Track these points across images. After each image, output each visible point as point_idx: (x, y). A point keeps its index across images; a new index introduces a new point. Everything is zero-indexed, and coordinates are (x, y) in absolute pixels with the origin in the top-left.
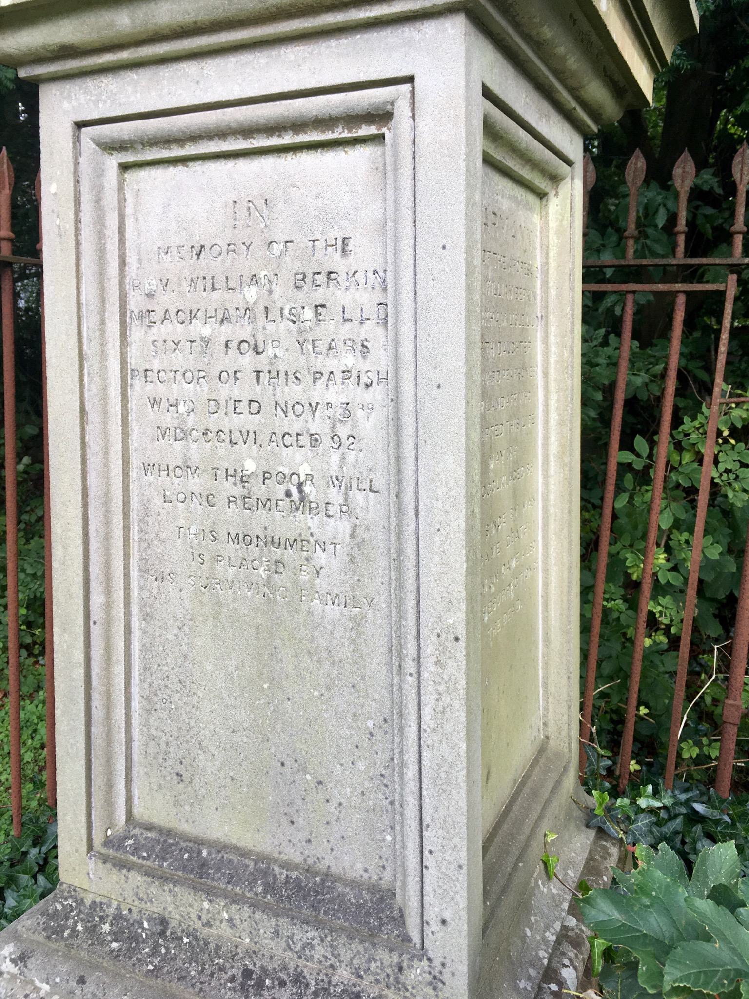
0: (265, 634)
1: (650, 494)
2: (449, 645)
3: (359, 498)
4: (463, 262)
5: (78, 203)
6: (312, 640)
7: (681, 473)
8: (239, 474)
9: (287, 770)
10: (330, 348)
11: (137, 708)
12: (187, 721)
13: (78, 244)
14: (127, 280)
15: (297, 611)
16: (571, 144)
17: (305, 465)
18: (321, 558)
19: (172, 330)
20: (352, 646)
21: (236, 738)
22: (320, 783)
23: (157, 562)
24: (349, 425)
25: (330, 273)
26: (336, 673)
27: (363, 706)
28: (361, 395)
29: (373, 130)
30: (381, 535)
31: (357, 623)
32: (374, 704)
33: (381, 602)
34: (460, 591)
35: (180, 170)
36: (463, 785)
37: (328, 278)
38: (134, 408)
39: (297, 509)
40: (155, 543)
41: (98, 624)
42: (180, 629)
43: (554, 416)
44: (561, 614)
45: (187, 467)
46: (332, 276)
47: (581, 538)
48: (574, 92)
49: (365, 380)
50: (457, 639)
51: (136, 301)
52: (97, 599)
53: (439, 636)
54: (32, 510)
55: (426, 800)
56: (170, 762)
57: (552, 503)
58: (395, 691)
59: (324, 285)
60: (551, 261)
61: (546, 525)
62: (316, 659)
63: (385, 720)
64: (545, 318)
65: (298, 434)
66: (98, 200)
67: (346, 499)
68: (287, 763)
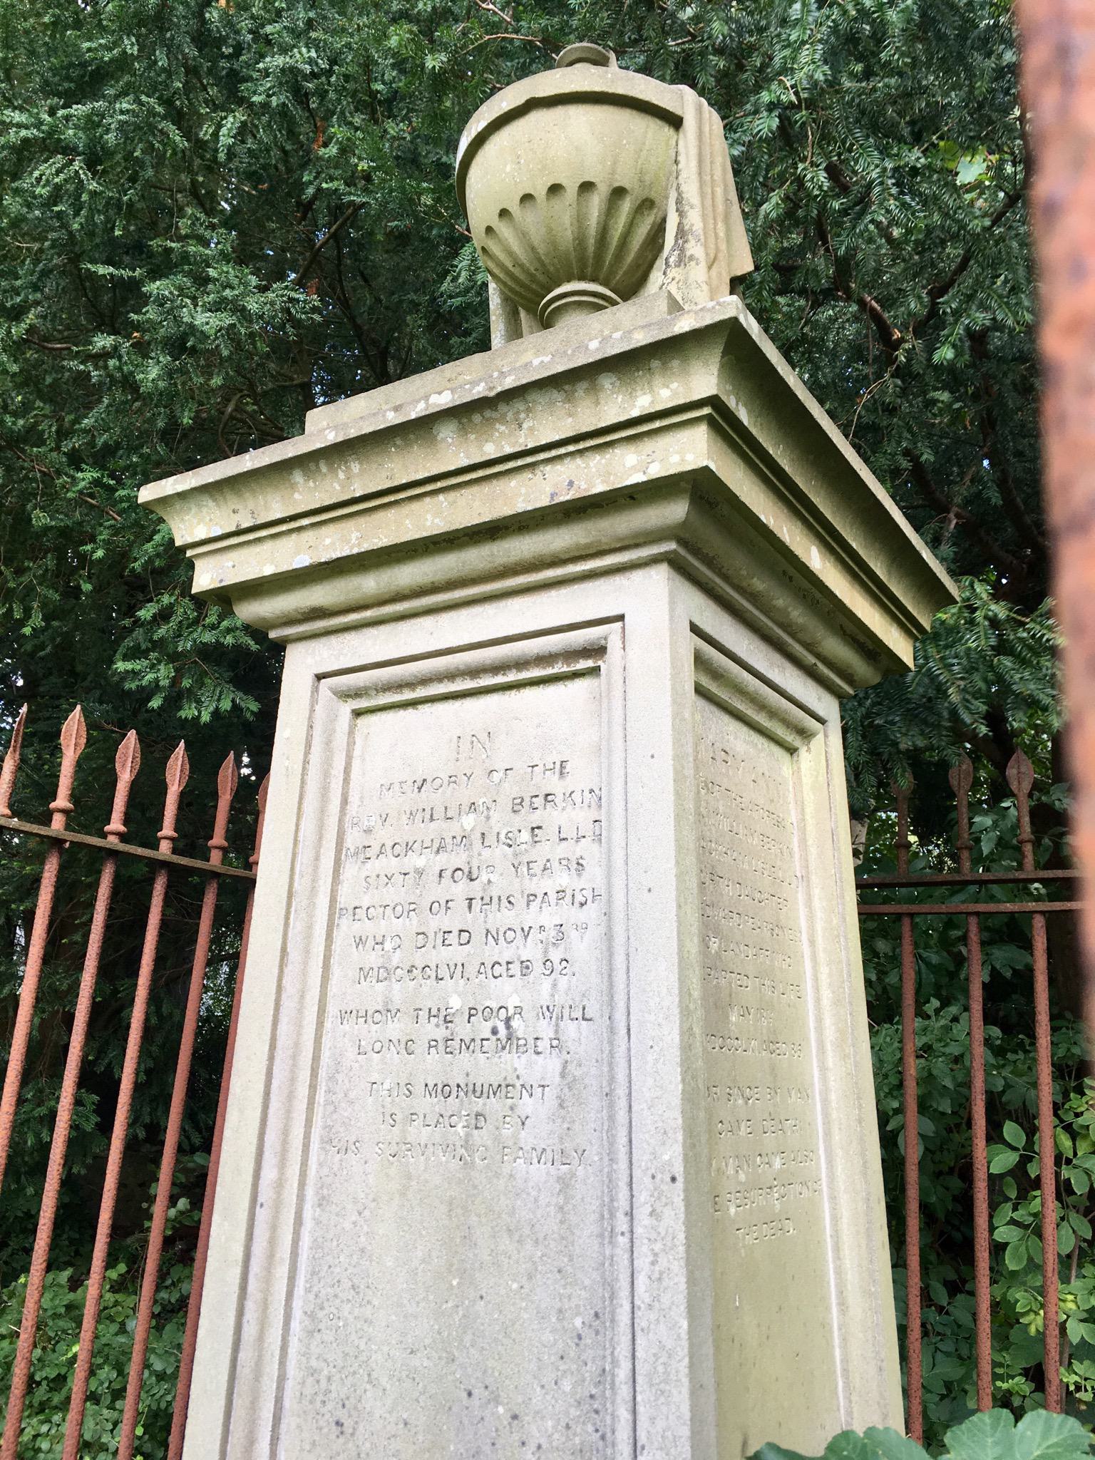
0: (460, 1211)
1: (1038, 1200)
2: (664, 1187)
3: (571, 1030)
4: (671, 768)
5: (308, 745)
6: (512, 1213)
7: (1075, 1167)
8: (443, 1013)
9: (475, 1402)
10: (545, 869)
11: (298, 1329)
12: (356, 1343)
13: (303, 782)
14: (347, 818)
15: (497, 1175)
16: (828, 706)
17: (515, 995)
18: (527, 1105)
19: (389, 864)
20: (559, 1216)
21: (415, 1362)
22: (515, 1417)
23: (342, 1130)
24: (561, 948)
25: (547, 795)
26: (539, 1254)
27: (570, 1297)
28: (574, 915)
29: (589, 663)
30: (593, 1071)
31: (565, 1184)
32: (583, 1293)
33: (593, 1155)
34: (675, 1118)
35: (410, 711)
36: (685, 1381)
37: (546, 800)
38: (338, 950)
39: (504, 1048)
40: (343, 1105)
41: (265, 1206)
42: (360, 1214)
43: (826, 995)
44: (860, 1266)
45: (388, 1011)
46: (550, 798)
47: (883, 1160)
48: (809, 647)
49: (579, 898)
50: (673, 1179)
51: (353, 839)
52: (269, 1174)
53: (653, 1177)
54: (173, 1284)
55: (640, 1409)
56: (330, 1406)
57: (834, 1105)
58: (605, 1264)
59: (541, 808)
60: (808, 817)
61: (828, 1134)
62: (516, 1237)
63: (596, 1315)
64: (806, 878)
65: (508, 963)
66: (328, 743)
67: (557, 1032)
68: (475, 1392)
